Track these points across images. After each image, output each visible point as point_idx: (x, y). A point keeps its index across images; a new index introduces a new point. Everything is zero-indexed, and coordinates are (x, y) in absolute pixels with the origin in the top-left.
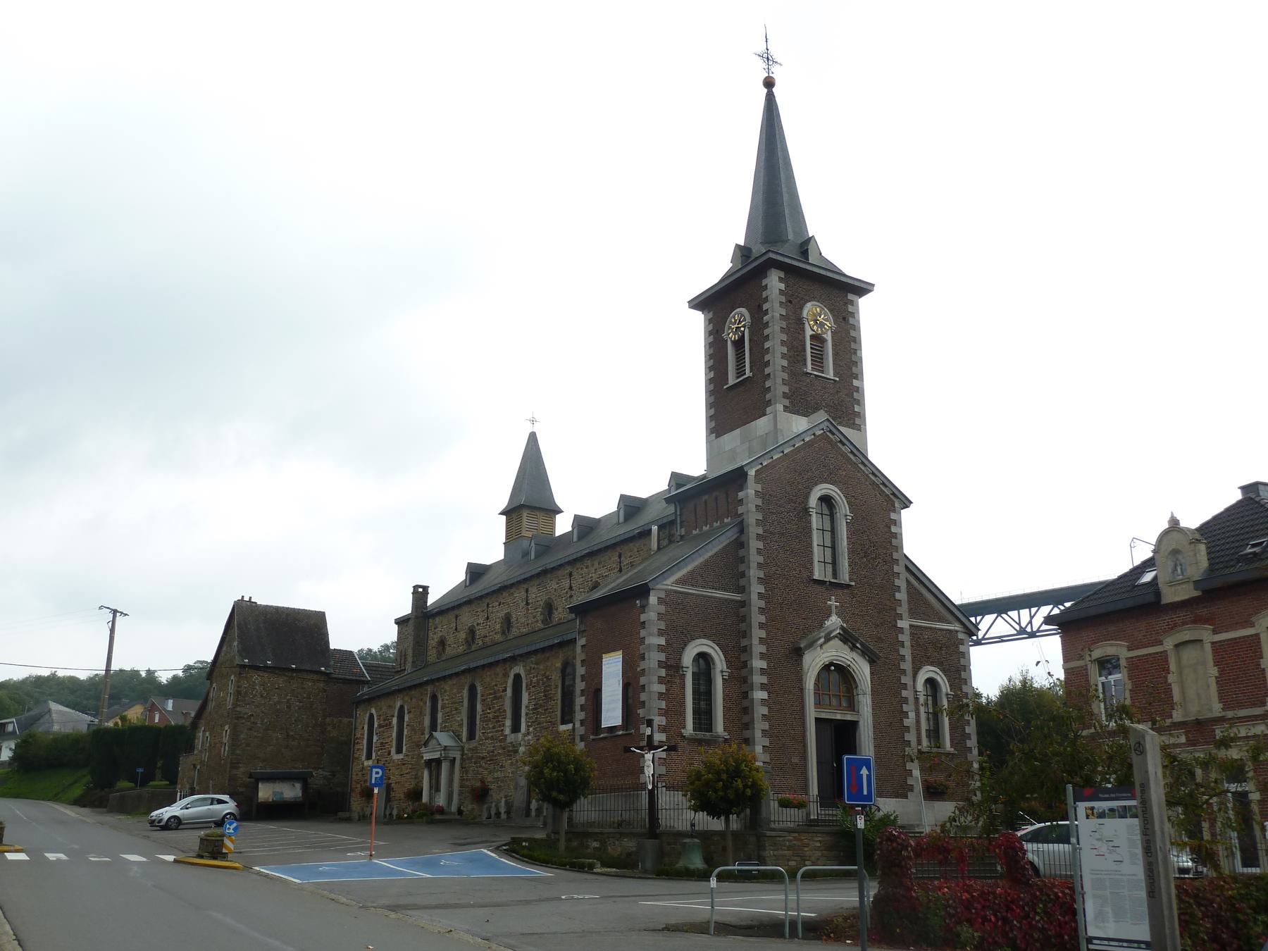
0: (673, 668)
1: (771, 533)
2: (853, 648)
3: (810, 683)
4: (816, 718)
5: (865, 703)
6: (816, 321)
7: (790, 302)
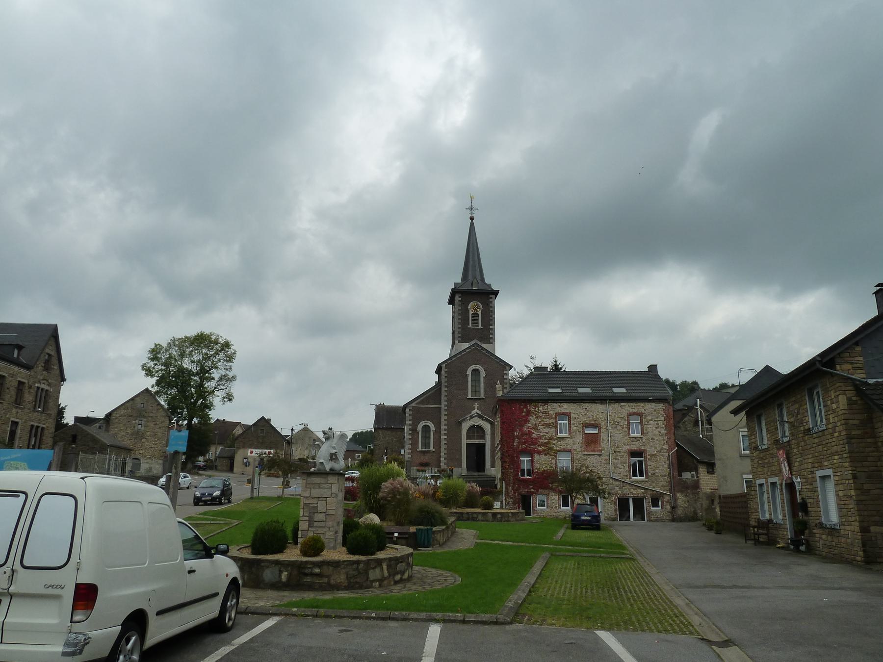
0: (414, 430)
2: (483, 420)
4: (467, 444)
5: (488, 437)
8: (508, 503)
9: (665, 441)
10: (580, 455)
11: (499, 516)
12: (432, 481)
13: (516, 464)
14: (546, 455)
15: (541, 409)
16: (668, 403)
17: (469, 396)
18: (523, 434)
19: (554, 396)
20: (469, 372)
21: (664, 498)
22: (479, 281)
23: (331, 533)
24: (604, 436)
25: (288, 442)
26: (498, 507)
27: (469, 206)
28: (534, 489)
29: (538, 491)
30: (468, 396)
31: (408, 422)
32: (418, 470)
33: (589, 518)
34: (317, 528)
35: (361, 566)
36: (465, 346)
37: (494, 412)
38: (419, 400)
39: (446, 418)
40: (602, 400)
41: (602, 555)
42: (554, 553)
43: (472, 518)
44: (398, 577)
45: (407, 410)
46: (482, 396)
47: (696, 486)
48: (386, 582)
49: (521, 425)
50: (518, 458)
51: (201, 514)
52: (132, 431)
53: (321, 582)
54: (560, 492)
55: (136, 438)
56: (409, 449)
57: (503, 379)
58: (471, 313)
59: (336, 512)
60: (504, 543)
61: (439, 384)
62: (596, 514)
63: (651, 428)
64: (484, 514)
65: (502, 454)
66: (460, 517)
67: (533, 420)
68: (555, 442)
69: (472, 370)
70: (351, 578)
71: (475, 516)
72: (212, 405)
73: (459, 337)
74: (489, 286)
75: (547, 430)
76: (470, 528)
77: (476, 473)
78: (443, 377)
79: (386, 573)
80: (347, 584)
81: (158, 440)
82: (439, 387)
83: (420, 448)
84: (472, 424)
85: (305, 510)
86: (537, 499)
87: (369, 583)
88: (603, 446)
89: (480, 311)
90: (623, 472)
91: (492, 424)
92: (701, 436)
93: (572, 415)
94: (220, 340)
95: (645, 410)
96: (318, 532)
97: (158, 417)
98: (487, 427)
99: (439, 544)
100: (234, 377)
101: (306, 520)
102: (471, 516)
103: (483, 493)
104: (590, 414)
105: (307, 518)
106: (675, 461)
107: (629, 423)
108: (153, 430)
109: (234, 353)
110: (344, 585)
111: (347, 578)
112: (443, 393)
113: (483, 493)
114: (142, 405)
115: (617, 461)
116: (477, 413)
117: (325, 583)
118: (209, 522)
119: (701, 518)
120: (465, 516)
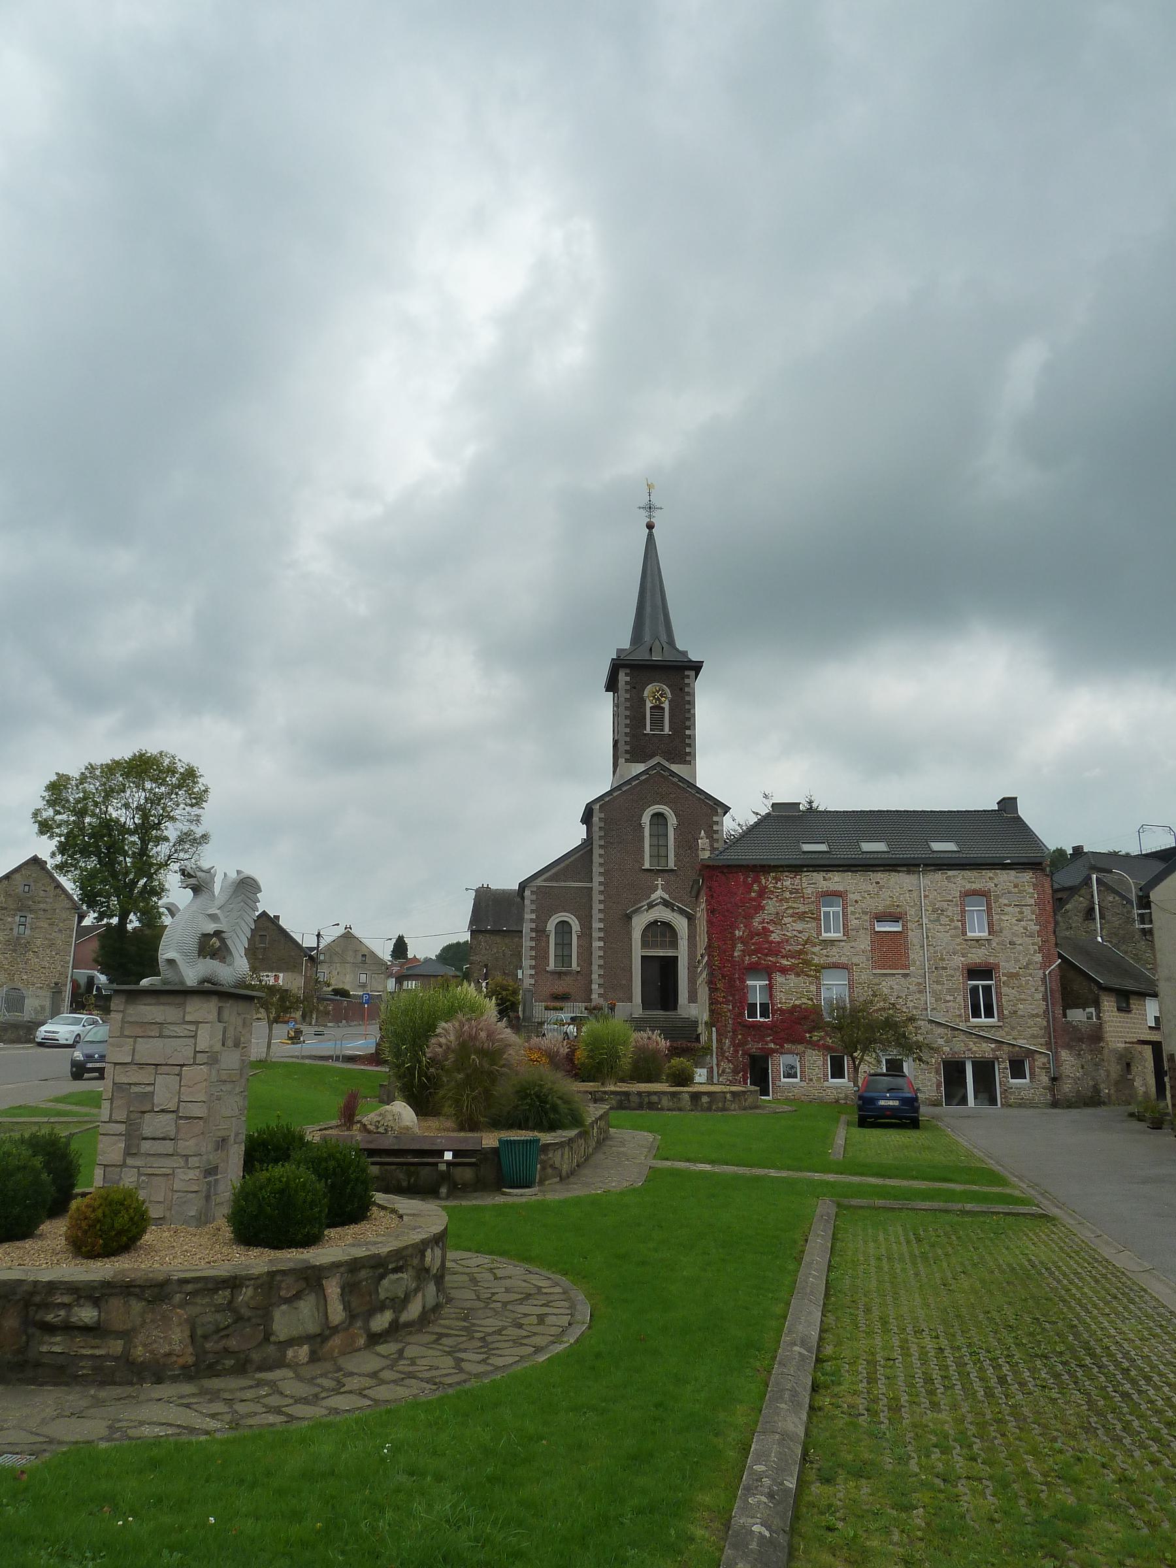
1: (611, 843)
2: (673, 910)
3: (637, 935)
6: (654, 697)
7: (635, 688)
8: (723, 1072)
9: (1036, 947)
10: (867, 974)
11: (705, 1099)
12: (572, 1029)
13: (737, 993)
14: (798, 975)
15: (788, 883)
16: (1043, 870)
17: (647, 866)
18: (752, 935)
19: (814, 858)
20: (646, 819)
21: (1034, 1060)
22: (665, 645)
23: (192, 1174)
24: (913, 936)
25: (311, 957)
26: (703, 1079)
27: (644, 501)
28: (775, 1044)
29: (782, 1047)
30: (643, 865)
31: (528, 916)
32: (547, 1008)
33: (896, 1103)
34: (152, 1159)
35: (246, 1294)
36: (639, 768)
37: (694, 893)
38: (550, 873)
39: (602, 907)
40: (910, 866)
41: (968, 1207)
42: (846, 1202)
43: (649, 1103)
44: (381, 1321)
45: (527, 893)
46: (671, 865)
47: (1096, 1036)
48: (336, 1341)
49: (749, 917)
50: (743, 981)
51: (57, 1100)
52: (7, 937)
53: (98, 1352)
54: (827, 1048)
55: (15, 951)
56: (532, 967)
57: (712, 833)
58: (649, 705)
59: (209, 1109)
60: (717, 1169)
61: (588, 843)
62: (909, 1095)
63: (1007, 919)
64: (674, 1094)
65: (711, 974)
66: (624, 1102)
67: (771, 906)
68: (816, 949)
69: (653, 816)
70: (205, 1337)
71: (655, 1098)
72: (163, 890)
73: (627, 752)
74: (685, 653)
75: (799, 926)
76: (642, 1128)
77: (662, 1012)
78: (595, 829)
79: (337, 1313)
80: (191, 1360)
81: (56, 954)
82: (589, 848)
83: (552, 966)
84: (652, 920)
85: (116, 1103)
86: (780, 1062)
87: (271, 1349)
88: (912, 956)
89: (667, 702)
90: (954, 1007)
91: (691, 918)
92: (1099, 939)
93: (851, 896)
94: (179, 764)
95: (996, 885)
96: (150, 1171)
97: (57, 911)
98: (681, 924)
99: (561, 1177)
100: (205, 837)
101: (120, 1134)
102: (646, 1100)
103: (675, 1052)
104: (885, 893)
105: (122, 1128)
106: (1056, 986)
107: (963, 912)
108: (48, 936)
109: (204, 791)
110: (181, 1361)
111: (192, 1337)
112: (597, 860)
113: (675, 1052)
114: (27, 888)
115: (939, 987)
116: (662, 898)
117: (116, 1359)
118: (46, 1119)
119: (1106, 1100)
120: (635, 1099)
